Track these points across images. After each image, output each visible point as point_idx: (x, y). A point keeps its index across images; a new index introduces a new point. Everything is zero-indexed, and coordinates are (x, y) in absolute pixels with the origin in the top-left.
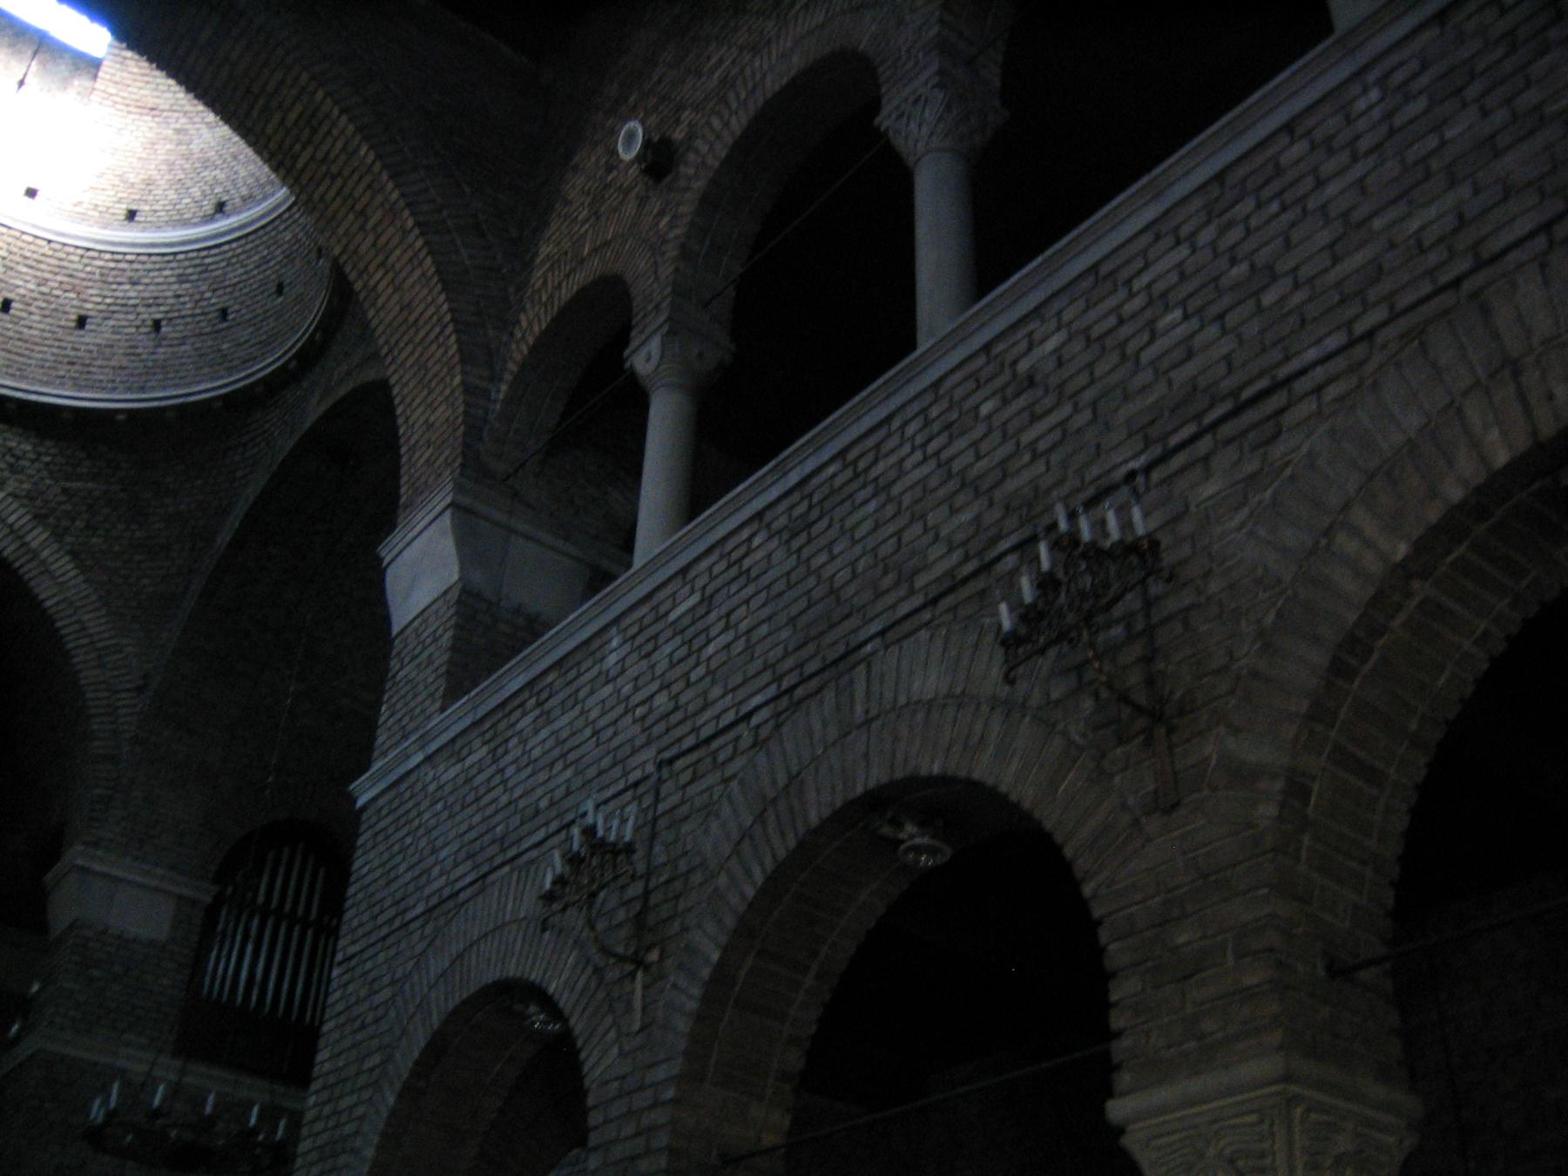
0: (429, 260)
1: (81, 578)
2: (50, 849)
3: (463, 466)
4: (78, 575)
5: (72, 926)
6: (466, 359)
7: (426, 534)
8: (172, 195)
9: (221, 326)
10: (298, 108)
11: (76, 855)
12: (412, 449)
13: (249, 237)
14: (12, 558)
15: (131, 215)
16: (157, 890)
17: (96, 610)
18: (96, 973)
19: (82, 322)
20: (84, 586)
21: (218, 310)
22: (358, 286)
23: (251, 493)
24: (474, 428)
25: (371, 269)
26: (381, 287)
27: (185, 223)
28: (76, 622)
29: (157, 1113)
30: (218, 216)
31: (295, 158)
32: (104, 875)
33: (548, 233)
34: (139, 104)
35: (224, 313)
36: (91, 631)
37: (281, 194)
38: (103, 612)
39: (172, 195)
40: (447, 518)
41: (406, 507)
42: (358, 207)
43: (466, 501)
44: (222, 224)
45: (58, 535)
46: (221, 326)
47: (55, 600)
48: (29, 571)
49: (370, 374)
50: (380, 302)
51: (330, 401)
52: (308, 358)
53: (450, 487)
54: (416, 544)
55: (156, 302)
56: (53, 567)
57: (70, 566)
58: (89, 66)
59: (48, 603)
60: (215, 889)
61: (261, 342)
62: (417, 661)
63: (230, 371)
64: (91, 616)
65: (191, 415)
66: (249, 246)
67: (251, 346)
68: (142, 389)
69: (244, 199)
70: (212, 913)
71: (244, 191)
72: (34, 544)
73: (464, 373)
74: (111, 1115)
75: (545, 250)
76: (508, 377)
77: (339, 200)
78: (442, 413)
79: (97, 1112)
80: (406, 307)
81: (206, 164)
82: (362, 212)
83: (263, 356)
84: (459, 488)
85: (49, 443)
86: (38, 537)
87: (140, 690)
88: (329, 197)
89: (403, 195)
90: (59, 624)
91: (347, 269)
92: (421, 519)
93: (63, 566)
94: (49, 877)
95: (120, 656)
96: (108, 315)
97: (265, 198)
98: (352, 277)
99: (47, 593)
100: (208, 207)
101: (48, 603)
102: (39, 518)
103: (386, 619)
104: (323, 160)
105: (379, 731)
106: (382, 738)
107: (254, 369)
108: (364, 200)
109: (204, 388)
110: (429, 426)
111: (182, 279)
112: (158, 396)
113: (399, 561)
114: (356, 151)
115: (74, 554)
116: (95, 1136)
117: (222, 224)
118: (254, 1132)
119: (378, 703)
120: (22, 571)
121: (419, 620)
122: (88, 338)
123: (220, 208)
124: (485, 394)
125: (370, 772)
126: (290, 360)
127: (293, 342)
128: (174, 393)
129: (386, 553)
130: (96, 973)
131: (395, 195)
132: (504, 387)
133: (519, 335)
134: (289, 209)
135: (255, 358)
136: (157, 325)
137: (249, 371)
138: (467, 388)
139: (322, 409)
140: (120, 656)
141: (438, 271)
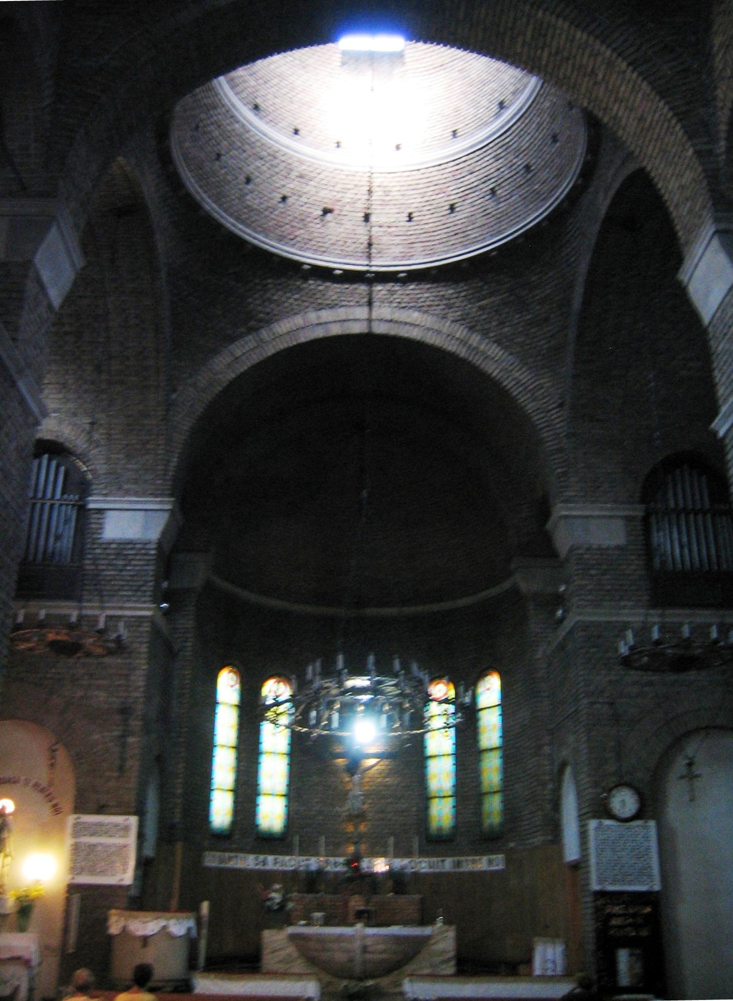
0: (645, 84)
1: (506, 354)
2: (544, 511)
3: (714, 205)
4: (504, 353)
5: (571, 550)
6: (691, 135)
7: (704, 259)
8: (472, 111)
9: (529, 176)
10: (530, 28)
11: (560, 510)
12: (677, 205)
13: (524, 116)
14: (467, 356)
15: (454, 133)
16: (611, 517)
17: (520, 369)
18: (593, 572)
19: (452, 208)
20: (510, 357)
21: (523, 168)
22: (606, 120)
23: (583, 268)
24: (712, 178)
25: (610, 104)
26: (620, 114)
27: (486, 124)
28: (513, 380)
29: (658, 643)
30: (502, 111)
31: (540, 59)
32: (580, 517)
33: (715, 28)
34: (434, 66)
35: (527, 168)
36: (523, 381)
37: (533, 81)
38: (524, 369)
39: (472, 111)
40: (715, 243)
41: (687, 243)
42: (589, 70)
43: (723, 226)
44: (507, 114)
45: (485, 333)
46: (529, 176)
47: (498, 371)
48: (477, 361)
49: (631, 167)
50: (623, 123)
51: (612, 193)
52: (587, 173)
53: (711, 221)
54: (701, 264)
55: (486, 179)
56: (489, 353)
57: (497, 350)
58: (398, 57)
59: (494, 374)
60: (643, 506)
61: (555, 176)
62: (727, 337)
63: (545, 200)
64: (520, 372)
65: (532, 235)
66: (527, 121)
67: (551, 180)
68: (500, 232)
69: (514, 93)
70: (646, 519)
71: (512, 89)
72: (475, 344)
73: (693, 145)
74: (632, 648)
75: (717, 41)
76: (723, 135)
77: (575, 73)
78: (688, 176)
79: (623, 650)
80: (641, 119)
81: (484, 83)
82: (593, 71)
83: (561, 183)
84: (717, 220)
85: (461, 285)
86: (475, 339)
87: (561, 405)
88: (568, 74)
89: (614, 50)
90: (505, 384)
91: (596, 112)
92: (698, 249)
93: (494, 351)
94: (549, 526)
95: (543, 390)
96: (464, 198)
97: (525, 87)
98: (600, 114)
99: (492, 369)
100: (495, 108)
101: (494, 374)
102: (471, 328)
103: (693, 316)
104: (557, 53)
105: (718, 388)
106: (721, 391)
107: (557, 194)
108: (591, 67)
109: (533, 217)
110: (682, 187)
111: (497, 158)
112: (511, 231)
113: (693, 280)
114: (574, 37)
115: (498, 342)
116: (626, 662)
117: (507, 114)
118: (716, 642)
119: (711, 371)
120: (474, 361)
121: (720, 311)
122: (459, 216)
123: (501, 105)
124: (710, 152)
125: (720, 416)
126: (577, 180)
127: (575, 167)
128: (519, 227)
129: (683, 276)
130: (593, 572)
131: (608, 53)
132: (723, 143)
133: (720, 104)
134: (542, 87)
135: (557, 186)
136: (493, 191)
137: (555, 196)
138: (699, 154)
139: (608, 202)
140: (543, 390)
141: (654, 88)
